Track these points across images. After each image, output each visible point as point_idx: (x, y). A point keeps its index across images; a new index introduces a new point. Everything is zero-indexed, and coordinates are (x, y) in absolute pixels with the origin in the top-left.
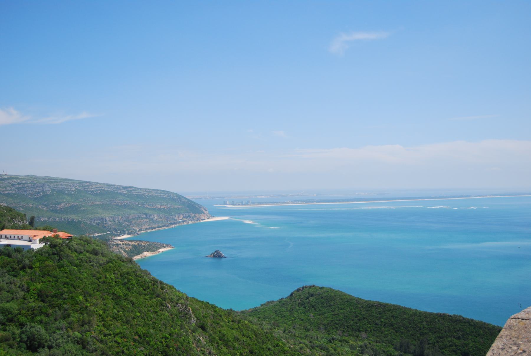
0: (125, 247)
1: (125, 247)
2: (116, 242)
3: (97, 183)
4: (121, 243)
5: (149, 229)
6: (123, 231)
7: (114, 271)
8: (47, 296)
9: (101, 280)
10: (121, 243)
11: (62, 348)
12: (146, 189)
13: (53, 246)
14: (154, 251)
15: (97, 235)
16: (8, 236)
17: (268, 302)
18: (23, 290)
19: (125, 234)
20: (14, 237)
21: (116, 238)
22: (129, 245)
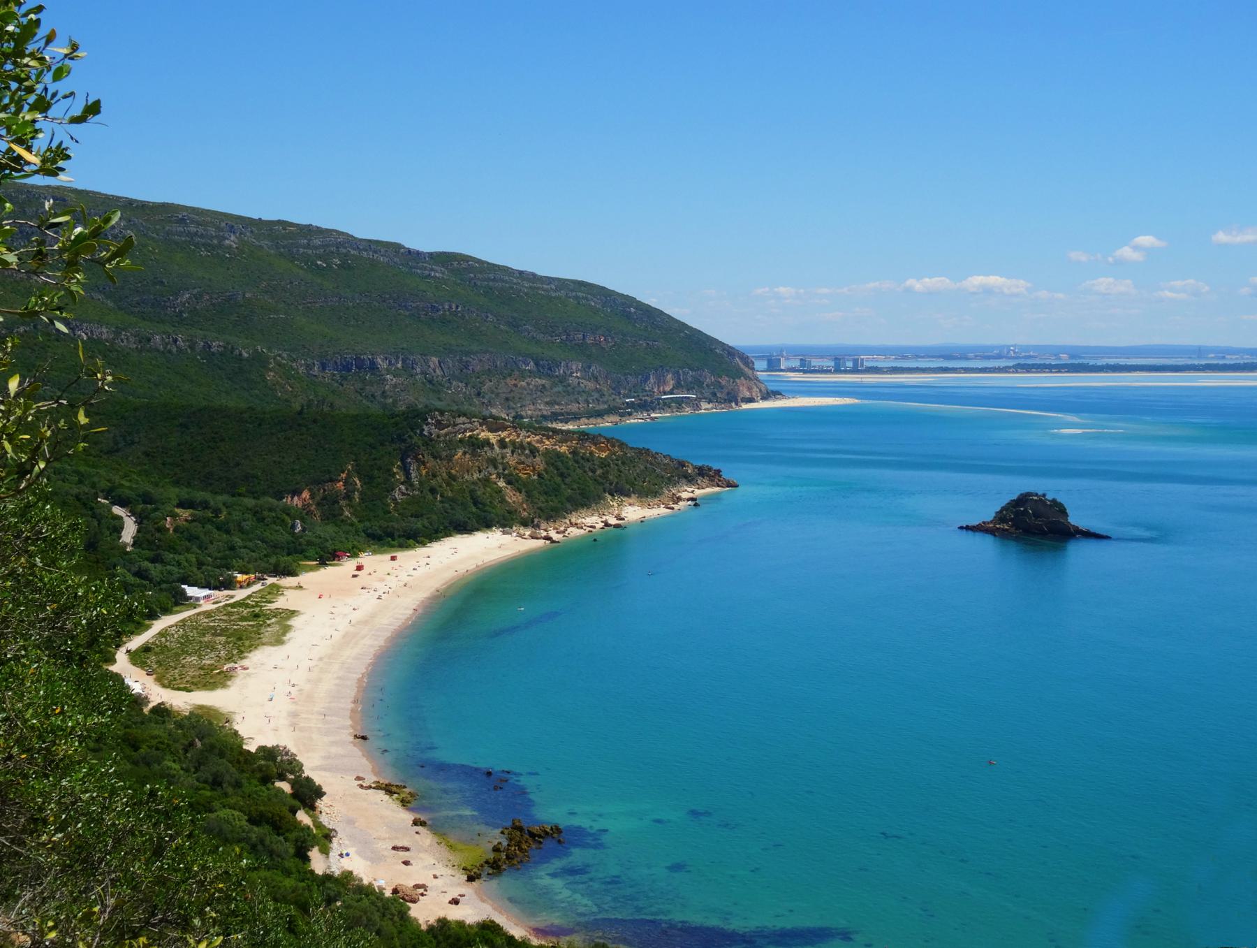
1: (511, 460)
4: (493, 438)
10: (493, 438)
12: (521, 272)
22: (534, 451)
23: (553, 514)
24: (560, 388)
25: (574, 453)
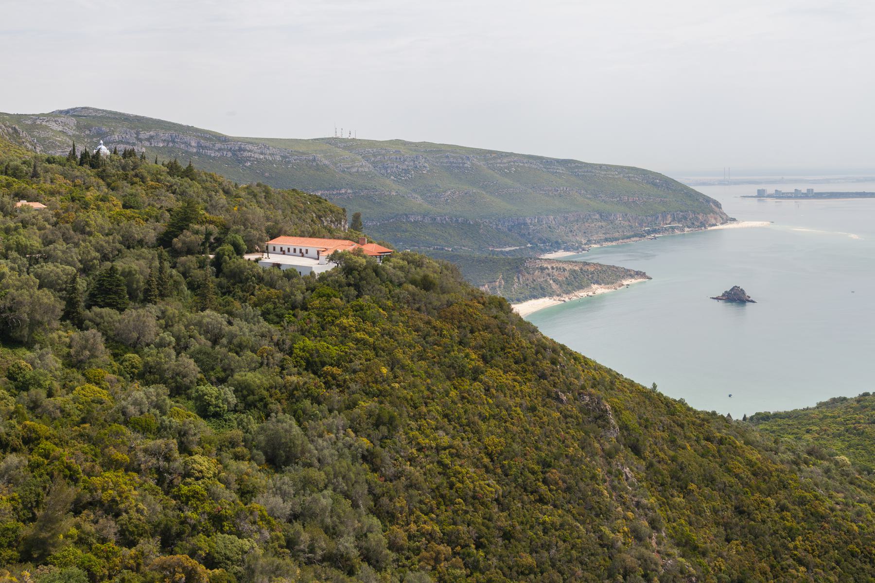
0: (556, 273)
1: (556, 273)
2: (539, 264)
3: (512, 154)
5: (606, 240)
6: (557, 242)
7: (459, 322)
8: (323, 364)
9: (430, 339)
11: (328, 469)
13: (349, 270)
14: (613, 283)
15: (508, 249)
16: (285, 249)
17: (834, 401)
18: (281, 350)
19: (559, 248)
20: (295, 250)
21: (542, 257)
22: (564, 270)
23: (568, 292)
24: (610, 226)
25: (581, 269)
